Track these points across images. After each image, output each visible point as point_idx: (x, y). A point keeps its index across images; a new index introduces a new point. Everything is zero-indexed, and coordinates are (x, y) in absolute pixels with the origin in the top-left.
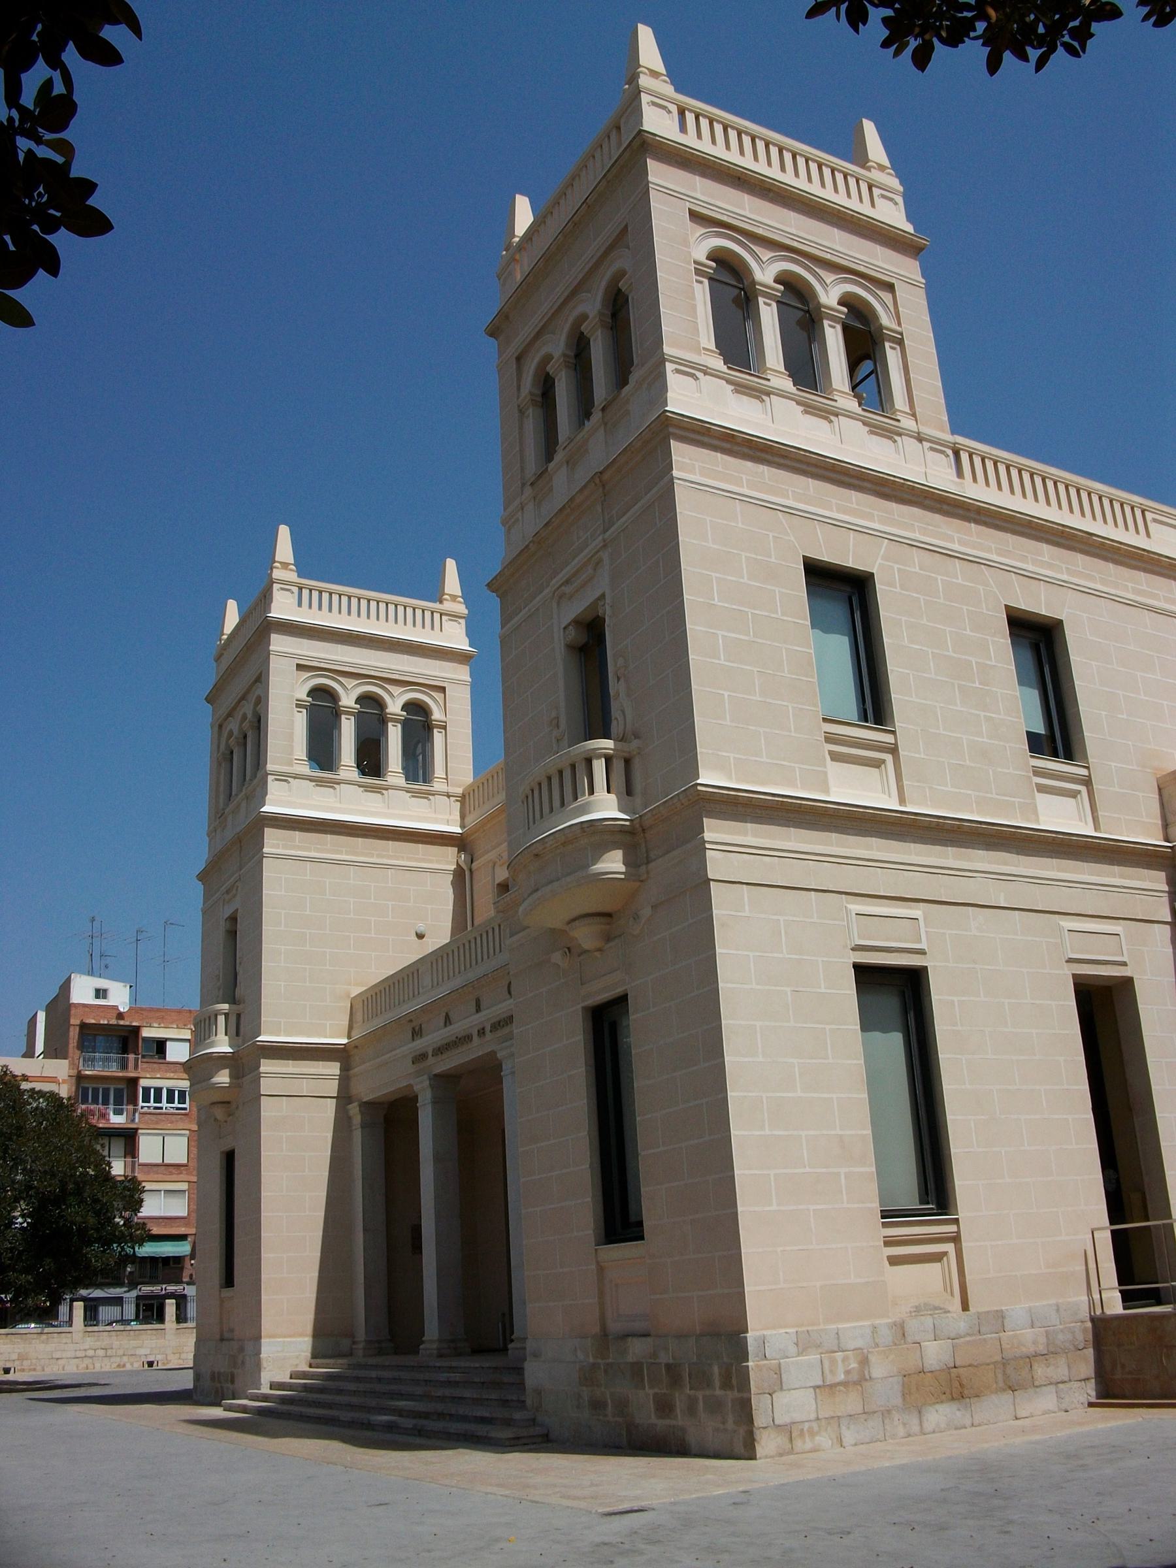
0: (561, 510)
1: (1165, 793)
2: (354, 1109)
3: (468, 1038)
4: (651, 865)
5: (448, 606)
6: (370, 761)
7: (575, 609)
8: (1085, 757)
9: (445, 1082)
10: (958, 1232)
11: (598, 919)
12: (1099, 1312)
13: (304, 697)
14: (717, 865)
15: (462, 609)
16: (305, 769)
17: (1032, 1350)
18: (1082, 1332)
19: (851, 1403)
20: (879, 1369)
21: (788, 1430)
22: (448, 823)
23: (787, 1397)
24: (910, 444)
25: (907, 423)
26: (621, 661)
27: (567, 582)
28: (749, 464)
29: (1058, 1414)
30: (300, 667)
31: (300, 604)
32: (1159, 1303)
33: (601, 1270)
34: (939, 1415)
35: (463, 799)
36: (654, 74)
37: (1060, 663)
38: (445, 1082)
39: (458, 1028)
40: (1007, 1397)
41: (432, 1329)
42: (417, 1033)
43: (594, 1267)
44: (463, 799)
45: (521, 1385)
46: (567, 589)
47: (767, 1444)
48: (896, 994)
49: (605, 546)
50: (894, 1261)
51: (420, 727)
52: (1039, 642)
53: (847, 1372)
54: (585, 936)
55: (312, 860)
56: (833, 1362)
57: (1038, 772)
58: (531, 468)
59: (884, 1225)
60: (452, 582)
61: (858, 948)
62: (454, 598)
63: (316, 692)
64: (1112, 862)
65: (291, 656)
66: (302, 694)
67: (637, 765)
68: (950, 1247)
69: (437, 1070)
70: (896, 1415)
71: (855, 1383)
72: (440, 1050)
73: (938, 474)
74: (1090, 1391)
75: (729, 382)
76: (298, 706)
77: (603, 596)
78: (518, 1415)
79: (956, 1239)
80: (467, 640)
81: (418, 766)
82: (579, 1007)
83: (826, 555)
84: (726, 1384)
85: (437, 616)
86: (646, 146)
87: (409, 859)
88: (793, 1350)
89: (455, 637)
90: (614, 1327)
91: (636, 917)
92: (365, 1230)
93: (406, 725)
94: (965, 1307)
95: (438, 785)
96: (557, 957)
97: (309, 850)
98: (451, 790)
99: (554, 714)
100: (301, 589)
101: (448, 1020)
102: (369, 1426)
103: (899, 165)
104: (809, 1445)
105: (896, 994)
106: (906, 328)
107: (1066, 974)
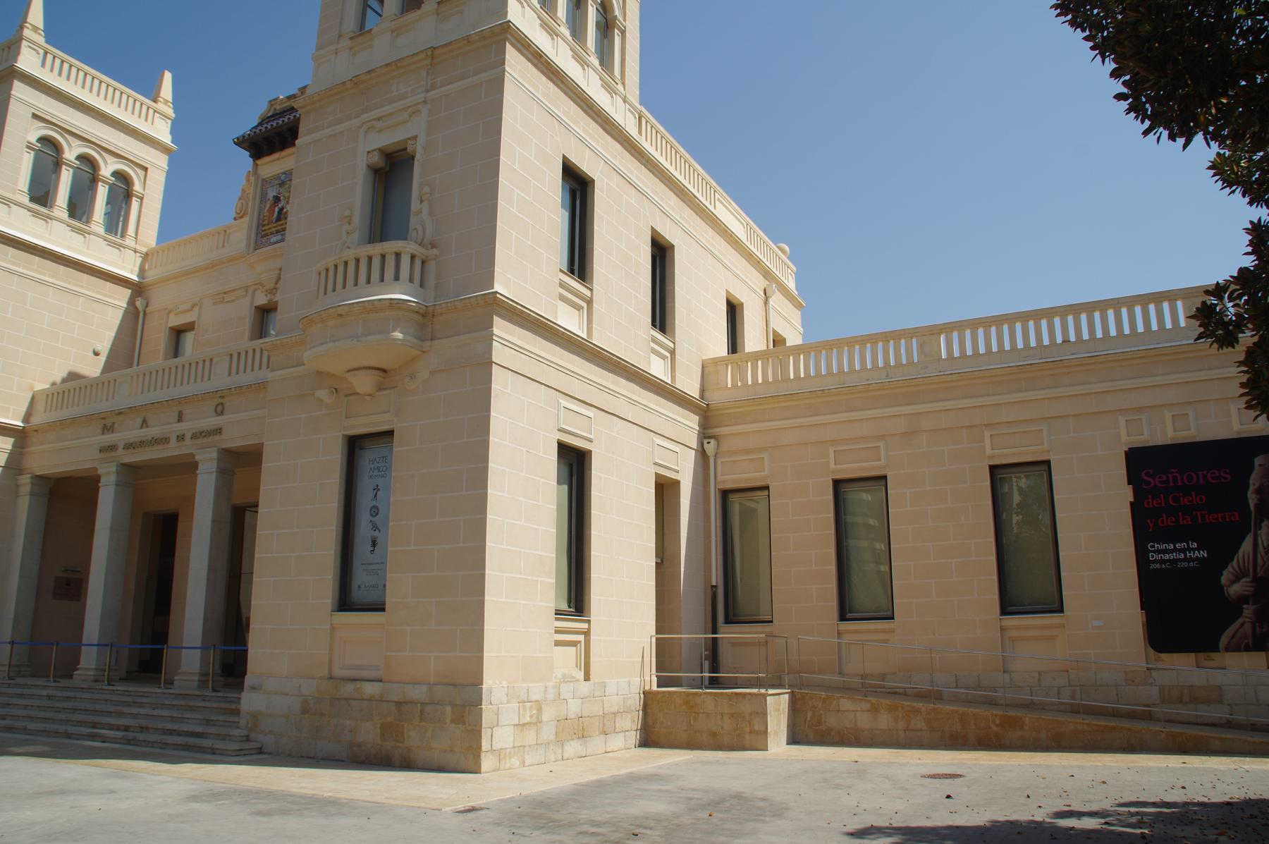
0: (386, 65)
1: (707, 370)
2: (25, 480)
3: (164, 441)
4: (436, 342)
5: (160, 106)
6: (79, 208)
7: (387, 139)
8: (673, 336)
9: (132, 474)
10: (589, 629)
11: (377, 372)
12: (647, 688)
13: (34, 140)
14: (499, 353)
15: (170, 112)
16: (25, 200)
17: (615, 709)
18: (636, 702)
19: (530, 737)
20: (549, 714)
21: (500, 754)
22: (132, 272)
23: (499, 733)
24: (620, 100)
25: (620, 87)
26: (427, 189)
27: (379, 119)
28: (544, 79)
29: (620, 754)
30: (35, 116)
31: (43, 65)
32: (681, 686)
33: (333, 628)
34: (572, 748)
35: (146, 257)
36: (35, 29)
37: (668, 272)
38: (132, 474)
39: (153, 431)
40: (603, 737)
41: (89, 658)
42: (107, 429)
43: (328, 627)
44: (146, 257)
45: (237, 712)
46: (379, 124)
47: (487, 763)
48: (575, 463)
49: (425, 102)
50: (558, 643)
51: (123, 190)
52: (661, 253)
53: (531, 716)
54: (363, 383)
55: (20, 275)
56: (525, 709)
57: (654, 340)
58: (351, 22)
59: (557, 619)
60: (167, 90)
61: (561, 430)
62: (166, 102)
63: (44, 140)
64: (679, 405)
65: (30, 105)
66: (33, 137)
67: (431, 266)
68: (581, 638)
69: (127, 460)
70: (552, 747)
71: (535, 724)
72: (130, 446)
73: (629, 125)
74: (634, 737)
75: (539, 17)
76: (28, 147)
77: (415, 138)
78: (236, 732)
79: (587, 634)
80: (170, 137)
81: (116, 222)
82: (340, 434)
83: (574, 159)
84: (460, 719)
85: (151, 111)
86: (14, 74)
87: (98, 292)
88: (505, 699)
89: (162, 131)
90: (338, 672)
91: (413, 377)
92: (21, 576)
93: (112, 188)
94: (587, 678)
95: (129, 241)
96: (323, 394)
97: (18, 265)
98: (139, 248)
99: (347, 213)
100: (46, 53)
101: (145, 423)
102: (25, 730)
103: (177, 102)
104: (508, 765)
105: (575, 463)
106: (628, 24)
107: (654, 470)
